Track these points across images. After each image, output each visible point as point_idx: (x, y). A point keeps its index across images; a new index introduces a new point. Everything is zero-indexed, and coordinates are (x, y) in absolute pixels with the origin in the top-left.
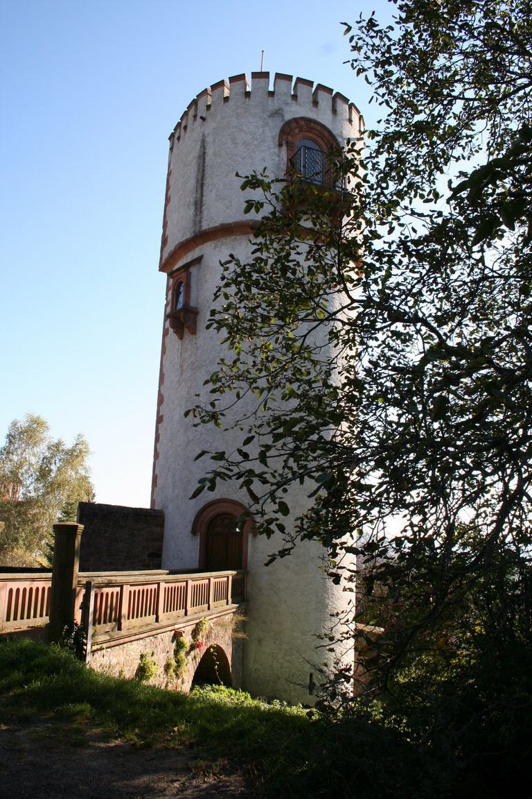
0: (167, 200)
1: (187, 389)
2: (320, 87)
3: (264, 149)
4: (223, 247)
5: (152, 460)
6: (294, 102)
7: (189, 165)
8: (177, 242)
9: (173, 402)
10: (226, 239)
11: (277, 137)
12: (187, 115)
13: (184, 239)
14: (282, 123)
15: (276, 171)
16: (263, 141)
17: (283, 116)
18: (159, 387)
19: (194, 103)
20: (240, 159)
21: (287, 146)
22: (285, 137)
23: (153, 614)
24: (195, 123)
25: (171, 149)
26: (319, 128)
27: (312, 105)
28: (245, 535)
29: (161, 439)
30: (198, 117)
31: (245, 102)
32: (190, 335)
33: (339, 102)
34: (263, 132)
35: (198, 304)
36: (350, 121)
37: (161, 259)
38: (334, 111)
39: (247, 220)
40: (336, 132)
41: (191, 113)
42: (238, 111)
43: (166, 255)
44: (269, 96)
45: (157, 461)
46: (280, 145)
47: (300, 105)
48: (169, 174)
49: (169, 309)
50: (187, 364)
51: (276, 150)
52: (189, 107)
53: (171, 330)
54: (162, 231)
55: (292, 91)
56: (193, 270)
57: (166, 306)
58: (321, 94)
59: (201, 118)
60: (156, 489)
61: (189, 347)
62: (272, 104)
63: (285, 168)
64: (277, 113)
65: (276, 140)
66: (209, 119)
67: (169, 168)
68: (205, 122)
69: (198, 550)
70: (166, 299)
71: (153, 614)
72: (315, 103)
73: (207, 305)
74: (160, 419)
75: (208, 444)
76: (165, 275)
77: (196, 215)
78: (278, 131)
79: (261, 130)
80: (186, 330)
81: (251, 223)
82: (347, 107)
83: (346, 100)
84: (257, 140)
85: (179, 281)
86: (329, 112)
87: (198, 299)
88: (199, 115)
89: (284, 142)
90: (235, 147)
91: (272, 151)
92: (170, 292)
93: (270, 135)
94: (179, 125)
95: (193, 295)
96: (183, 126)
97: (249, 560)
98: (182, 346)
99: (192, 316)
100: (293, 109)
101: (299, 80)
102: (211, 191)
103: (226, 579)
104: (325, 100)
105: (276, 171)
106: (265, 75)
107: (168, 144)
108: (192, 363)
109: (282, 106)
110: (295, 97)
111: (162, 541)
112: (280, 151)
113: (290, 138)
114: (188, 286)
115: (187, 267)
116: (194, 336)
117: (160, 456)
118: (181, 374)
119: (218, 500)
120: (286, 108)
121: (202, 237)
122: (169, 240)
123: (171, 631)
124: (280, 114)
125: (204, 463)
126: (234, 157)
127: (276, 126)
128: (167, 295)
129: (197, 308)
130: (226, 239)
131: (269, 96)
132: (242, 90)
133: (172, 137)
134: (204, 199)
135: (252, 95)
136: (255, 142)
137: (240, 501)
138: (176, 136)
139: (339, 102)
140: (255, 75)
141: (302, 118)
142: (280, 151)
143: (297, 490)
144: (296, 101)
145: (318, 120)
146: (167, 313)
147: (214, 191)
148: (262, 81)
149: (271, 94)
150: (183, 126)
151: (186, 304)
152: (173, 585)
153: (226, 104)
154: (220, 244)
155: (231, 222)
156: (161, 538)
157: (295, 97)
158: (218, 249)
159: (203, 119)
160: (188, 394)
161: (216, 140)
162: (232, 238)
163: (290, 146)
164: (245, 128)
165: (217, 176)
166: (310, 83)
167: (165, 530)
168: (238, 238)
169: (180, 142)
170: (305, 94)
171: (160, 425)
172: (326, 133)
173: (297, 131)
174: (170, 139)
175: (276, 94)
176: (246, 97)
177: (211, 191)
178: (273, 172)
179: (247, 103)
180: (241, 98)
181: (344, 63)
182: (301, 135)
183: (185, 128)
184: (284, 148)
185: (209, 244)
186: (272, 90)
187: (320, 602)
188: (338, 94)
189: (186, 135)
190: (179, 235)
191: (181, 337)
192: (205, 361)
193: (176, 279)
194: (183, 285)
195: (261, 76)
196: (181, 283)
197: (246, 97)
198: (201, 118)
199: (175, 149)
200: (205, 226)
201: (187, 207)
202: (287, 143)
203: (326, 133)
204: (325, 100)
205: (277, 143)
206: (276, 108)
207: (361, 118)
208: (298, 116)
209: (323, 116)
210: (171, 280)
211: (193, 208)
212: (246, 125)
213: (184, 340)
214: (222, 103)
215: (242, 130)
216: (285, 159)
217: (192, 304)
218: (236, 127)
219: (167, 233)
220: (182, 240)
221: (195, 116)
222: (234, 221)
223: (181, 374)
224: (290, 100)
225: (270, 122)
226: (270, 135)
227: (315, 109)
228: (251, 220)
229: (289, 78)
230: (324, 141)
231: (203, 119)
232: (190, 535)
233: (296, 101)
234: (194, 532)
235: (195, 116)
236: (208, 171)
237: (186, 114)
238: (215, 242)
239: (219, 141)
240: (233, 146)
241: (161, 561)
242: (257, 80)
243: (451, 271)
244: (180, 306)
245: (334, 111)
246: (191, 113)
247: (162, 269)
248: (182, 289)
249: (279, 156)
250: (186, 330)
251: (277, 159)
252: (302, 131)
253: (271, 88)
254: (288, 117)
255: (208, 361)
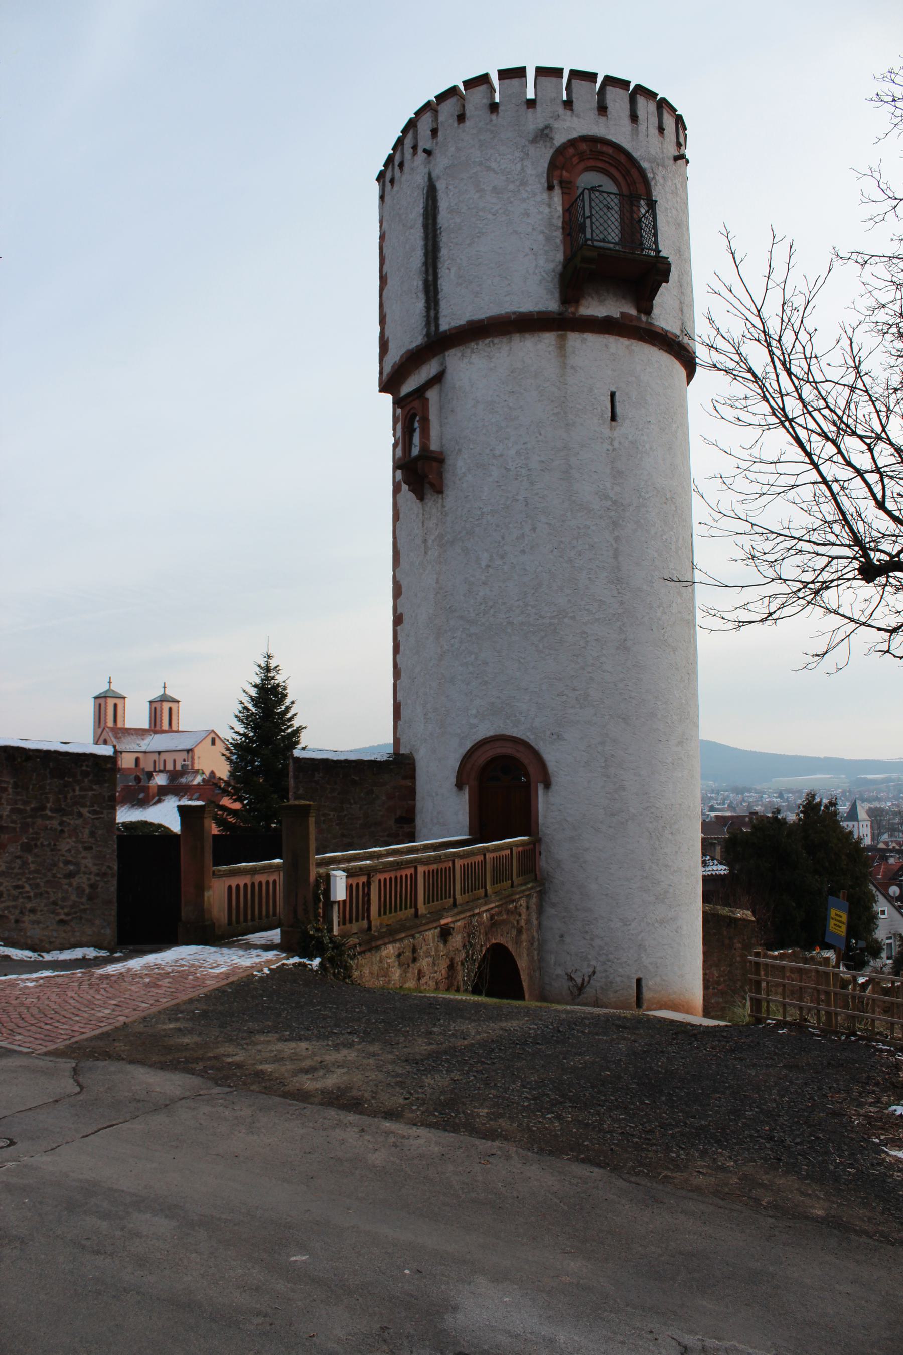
0: (383, 279)
1: (435, 576)
2: (610, 81)
3: (525, 195)
4: (473, 356)
5: (392, 681)
6: (569, 113)
7: (411, 228)
8: (403, 351)
9: (416, 595)
10: (477, 344)
11: (545, 175)
12: (403, 144)
13: (414, 345)
14: (551, 151)
15: (547, 231)
16: (524, 183)
17: (552, 139)
18: (394, 570)
19: (411, 125)
20: (490, 216)
21: (562, 188)
22: (557, 173)
23: (411, 907)
24: (416, 157)
25: (382, 197)
26: (610, 150)
27: (597, 113)
28: (532, 785)
29: (402, 648)
30: (420, 150)
31: (491, 121)
32: (436, 496)
33: (641, 101)
34: (522, 169)
35: (442, 446)
36: (661, 130)
37: (381, 373)
38: (634, 118)
39: (507, 313)
40: (639, 154)
41: (408, 142)
42: (482, 138)
43: (388, 369)
44: (528, 108)
45: (398, 682)
46: (550, 188)
47: (578, 117)
48: (382, 238)
49: (399, 452)
50: (433, 538)
51: (545, 196)
52: (405, 131)
53: (405, 487)
54: (378, 329)
55: (565, 93)
56: (432, 395)
57: (395, 446)
58: (612, 93)
59: (425, 151)
60: (400, 723)
61: (434, 511)
62: (534, 121)
63: (560, 225)
64: (544, 134)
65: (544, 180)
66: (437, 152)
67: (381, 227)
68: (431, 158)
69: (467, 811)
70: (394, 435)
71: (411, 907)
72: (602, 109)
73: (457, 448)
74: (398, 620)
75: (473, 657)
76: (388, 398)
77: (428, 308)
78: (546, 165)
79: (519, 166)
80: (427, 486)
81: (513, 317)
82: (652, 107)
83: (651, 95)
84: (513, 182)
85: (412, 411)
86: (626, 121)
87: (442, 439)
88: (422, 145)
89: (555, 182)
90: (480, 197)
91: (538, 198)
92: (399, 426)
93: (534, 172)
94: (390, 160)
95: (434, 432)
96: (397, 163)
97: (541, 820)
98: (424, 511)
99: (435, 464)
100: (568, 124)
101: (574, 74)
102: (449, 269)
103: (508, 852)
104: (617, 101)
105: (547, 231)
106: (520, 72)
107: (376, 187)
108: (441, 536)
109: (551, 122)
110: (568, 104)
111: (414, 800)
112: (550, 198)
113: (565, 173)
114: (425, 421)
115: (420, 393)
116: (440, 496)
117: (403, 675)
118: (426, 553)
119: (491, 737)
120: (556, 125)
121: (439, 342)
122: (391, 346)
123: (436, 928)
124: (547, 135)
125: (468, 684)
126: (481, 214)
127: (543, 155)
128: (394, 429)
129: (441, 453)
130: (477, 344)
131: (528, 108)
132: (486, 102)
133: (381, 177)
134: (440, 282)
135: (501, 108)
136: (511, 187)
137: (523, 737)
138: (388, 176)
139: (641, 101)
140: (504, 74)
141: (584, 139)
142: (550, 198)
143: (606, 717)
144: (572, 110)
145: (609, 137)
146: (397, 457)
147: (453, 270)
148: (515, 82)
149: (531, 104)
150: (397, 163)
151: (425, 447)
152: (435, 866)
153: (461, 125)
154: (469, 351)
155: (483, 316)
156: (411, 793)
157: (568, 104)
158: (466, 360)
159: (428, 152)
160: (437, 582)
161: (450, 187)
162: (487, 341)
163: (567, 187)
164: (494, 165)
165: (457, 244)
166: (592, 77)
167: (418, 783)
168: (496, 340)
169: (396, 188)
170: (586, 96)
171: (399, 628)
172: (622, 159)
173: (575, 160)
174: (378, 179)
175: (538, 101)
176: (492, 113)
177: (449, 269)
178: (542, 232)
179: (494, 122)
180: (485, 113)
181: (613, 395)
182: (582, 166)
183: (401, 165)
184: (557, 191)
185: (452, 352)
186: (533, 97)
187: (646, 878)
188: (639, 88)
189: (404, 178)
190: (410, 337)
191: (421, 497)
192: (460, 533)
193: (408, 408)
194: (418, 418)
195: (514, 74)
196: (415, 415)
197: (492, 113)
198: (425, 151)
199: (387, 198)
200: (444, 326)
201: (414, 296)
202: (561, 183)
203: (622, 159)
204: (617, 101)
205: (546, 185)
206: (541, 126)
207: (679, 120)
208: (575, 135)
209: (616, 130)
210: (399, 411)
211: (422, 296)
212: (495, 161)
213: (427, 501)
214: (456, 124)
215: (489, 168)
216: (560, 209)
217: (434, 446)
218: (480, 164)
219: (387, 334)
220: (411, 347)
221: (415, 147)
222: (487, 315)
223: (426, 553)
224: (561, 110)
225: (532, 149)
226: (534, 172)
227: (603, 120)
228: (514, 313)
229: (558, 72)
230: (621, 172)
231: (428, 152)
232: (455, 789)
233: (572, 110)
234: (459, 785)
235: (415, 147)
236: (444, 239)
237: (399, 142)
238: (461, 348)
239: (455, 187)
240: (477, 195)
241: (414, 827)
242: (507, 81)
243: (732, 922)
244: (415, 451)
245: (634, 118)
246: (408, 142)
247: (384, 389)
248: (416, 425)
249: (549, 206)
250: (427, 486)
251: (547, 210)
252: (584, 160)
253: (530, 94)
254: (560, 139)
255: (464, 533)
